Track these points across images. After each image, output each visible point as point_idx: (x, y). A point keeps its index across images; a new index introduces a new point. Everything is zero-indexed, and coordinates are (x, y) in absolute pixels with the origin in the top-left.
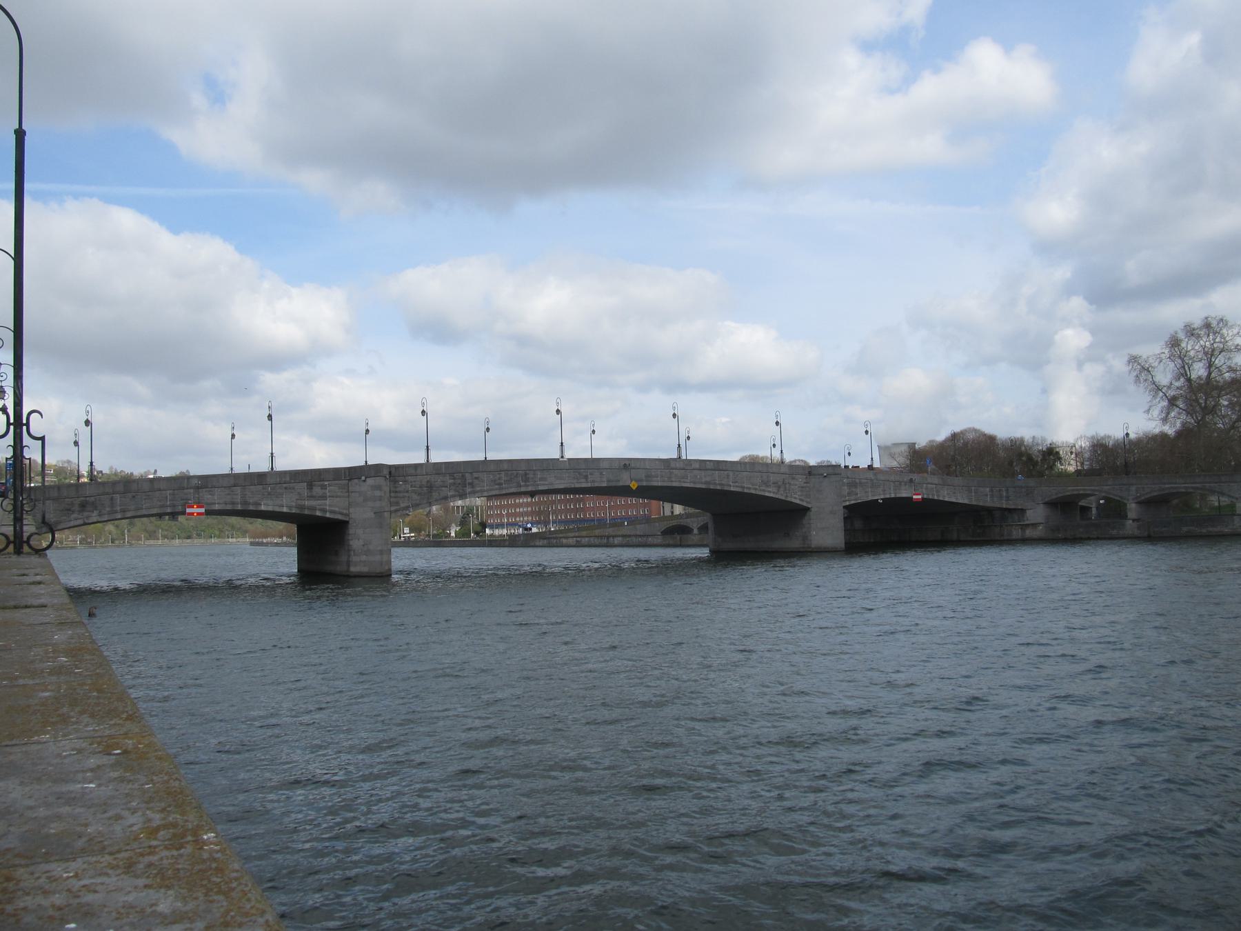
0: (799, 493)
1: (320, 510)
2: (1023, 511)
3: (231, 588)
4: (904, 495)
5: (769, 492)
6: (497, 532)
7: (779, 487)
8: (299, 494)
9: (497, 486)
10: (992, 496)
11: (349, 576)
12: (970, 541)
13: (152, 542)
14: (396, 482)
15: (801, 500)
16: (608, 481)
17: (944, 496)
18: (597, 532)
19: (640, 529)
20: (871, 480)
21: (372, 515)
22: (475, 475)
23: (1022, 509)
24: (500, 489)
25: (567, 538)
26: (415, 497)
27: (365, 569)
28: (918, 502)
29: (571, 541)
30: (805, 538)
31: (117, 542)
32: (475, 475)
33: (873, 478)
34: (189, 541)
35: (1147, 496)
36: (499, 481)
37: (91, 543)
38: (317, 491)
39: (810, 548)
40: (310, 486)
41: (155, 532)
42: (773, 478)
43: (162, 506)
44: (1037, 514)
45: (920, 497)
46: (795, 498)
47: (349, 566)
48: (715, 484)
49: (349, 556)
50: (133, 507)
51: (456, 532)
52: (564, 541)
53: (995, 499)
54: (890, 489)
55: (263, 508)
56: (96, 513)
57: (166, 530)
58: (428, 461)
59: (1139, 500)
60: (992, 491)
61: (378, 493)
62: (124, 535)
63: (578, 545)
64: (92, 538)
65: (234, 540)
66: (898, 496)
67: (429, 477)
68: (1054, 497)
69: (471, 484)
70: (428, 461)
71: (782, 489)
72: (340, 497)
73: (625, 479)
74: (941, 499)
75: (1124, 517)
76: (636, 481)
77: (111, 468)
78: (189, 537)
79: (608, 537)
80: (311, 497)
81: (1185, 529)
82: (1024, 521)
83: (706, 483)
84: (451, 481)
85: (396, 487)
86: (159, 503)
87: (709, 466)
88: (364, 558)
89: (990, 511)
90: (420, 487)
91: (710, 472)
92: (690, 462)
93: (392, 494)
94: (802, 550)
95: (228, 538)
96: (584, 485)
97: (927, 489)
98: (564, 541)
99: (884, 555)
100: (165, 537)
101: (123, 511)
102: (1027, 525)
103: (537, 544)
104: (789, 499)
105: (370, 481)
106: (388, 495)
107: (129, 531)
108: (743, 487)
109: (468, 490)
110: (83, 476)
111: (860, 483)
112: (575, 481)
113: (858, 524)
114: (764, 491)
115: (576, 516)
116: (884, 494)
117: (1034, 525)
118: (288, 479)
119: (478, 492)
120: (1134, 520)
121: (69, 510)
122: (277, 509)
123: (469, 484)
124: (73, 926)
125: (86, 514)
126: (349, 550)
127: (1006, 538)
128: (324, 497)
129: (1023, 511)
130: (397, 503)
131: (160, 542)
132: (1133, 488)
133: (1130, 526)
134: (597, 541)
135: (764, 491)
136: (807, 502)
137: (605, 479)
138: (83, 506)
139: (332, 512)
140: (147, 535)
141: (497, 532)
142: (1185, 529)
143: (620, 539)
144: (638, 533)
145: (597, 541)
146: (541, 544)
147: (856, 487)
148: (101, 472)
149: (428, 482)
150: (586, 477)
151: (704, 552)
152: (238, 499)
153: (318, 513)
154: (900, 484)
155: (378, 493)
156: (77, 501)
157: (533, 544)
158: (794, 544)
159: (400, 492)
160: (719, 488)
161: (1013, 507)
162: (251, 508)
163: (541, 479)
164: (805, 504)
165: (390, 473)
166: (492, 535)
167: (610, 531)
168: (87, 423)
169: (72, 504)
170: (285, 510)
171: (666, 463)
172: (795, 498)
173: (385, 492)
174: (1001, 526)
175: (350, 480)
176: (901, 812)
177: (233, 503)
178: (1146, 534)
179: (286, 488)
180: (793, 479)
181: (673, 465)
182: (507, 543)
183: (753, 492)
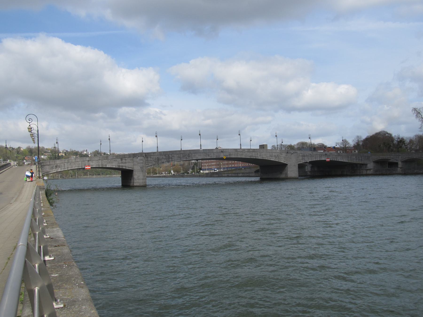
0: (283, 159)
1: (125, 167)
2: (366, 164)
3: (95, 189)
4: (323, 159)
5: (273, 159)
6: (205, 172)
7: (276, 157)
8: (118, 162)
9: (180, 159)
10: (356, 159)
11: (134, 186)
12: (351, 175)
13: (86, 177)
14: (147, 158)
15: (284, 161)
16: (216, 156)
17: (339, 160)
18: (234, 172)
19: (248, 171)
20: (311, 154)
21: (140, 168)
22: (173, 155)
23: (366, 164)
24: (180, 159)
25: (224, 174)
26: (154, 162)
27: (138, 184)
28: (328, 162)
29: (226, 175)
30: (286, 174)
31: (73, 177)
32: (173, 155)
33: (311, 153)
34: (99, 176)
35: (404, 160)
36: (180, 157)
37: (64, 177)
38: (124, 161)
39: (288, 177)
40: (122, 160)
41: (87, 173)
42: (274, 154)
43: (78, 166)
44: (371, 165)
45: (329, 160)
46: (282, 161)
47: (134, 183)
48: (253, 157)
49: (134, 180)
50: (70, 167)
51: (191, 171)
52: (223, 175)
53: (357, 160)
54: (318, 157)
55: (108, 166)
56: (60, 169)
57: (91, 172)
58: (158, 151)
59: (402, 161)
60: (356, 157)
61: (141, 161)
62: (76, 174)
63: (228, 176)
64: (64, 175)
65: (115, 175)
66: (321, 159)
67: (158, 156)
68: (376, 160)
69: (171, 158)
70: (158, 151)
71: (277, 158)
72: (131, 163)
73: (222, 156)
74: (338, 160)
75: (397, 166)
76: (225, 156)
77: (71, 149)
78: (99, 175)
79: (237, 173)
80: (122, 163)
81: (416, 171)
82: (367, 168)
83: (250, 156)
84: (165, 157)
85: (148, 159)
86: (78, 166)
87: (251, 151)
88: (138, 181)
89: (356, 164)
90: (155, 159)
91: (251, 153)
92: (160, 152)
93: (147, 162)
94: (285, 178)
95: (113, 175)
96: (208, 158)
97: (332, 157)
98: (223, 175)
99: (338, 178)
100: (90, 175)
101: (68, 168)
102: (368, 169)
103: (215, 176)
104: (280, 161)
105: (139, 158)
106: (145, 162)
107: (77, 173)
108: (263, 158)
109: (170, 160)
110: (60, 153)
111: (307, 156)
112: (205, 156)
113: (316, 169)
114: (271, 158)
115: (235, 165)
116: (316, 159)
117: (370, 169)
118: (115, 158)
119: (173, 160)
120: (400, 168)
121: (52, 168)
122: (112, 167)
123: (171, 158)
124: (82, 283)
125: (57, 169)
126: (134, 179)
127: (361, 174)
128: (126, 163)
129: (366, 164)
130: (148, 164)
131: (88, 177)
132: (400, 157)
133: (399, 170)
134: (234, 175)
135: (271, 158)
136: (286, 162)
137: (215, 156)
138: (56, 167)
139: (128, 167)
140: (84, 174)
141: (205, 172)
142: (416, 171)
143: (241, 174)
144: (247, 172)
145: (234, 175)
146: (216, 176)
147: (305, 157)
148: (67, 151)
149: (158, 158)
150: (209, 155)
151: (258, 179)
152: (100, 164)
153: (124, 168)
154: (322, 156)
155: (141, 161)
156: (55, 166)
157: (213, 176)
158: (283, 176)
159: (149, 161)
160: (254, 158)
161: (363, 163)
162: (104, 166)
163: (194, 156)
164: (285, 163)
165: (146, 155)
166: (203, 173)
167: (238, 171)
168: (57, 143)
169: (53, 166)
170: (114, 167)
171: (236, 150)
172: (282, 161)
173: (144, 161)
174: (360, 170)
175: (133, 157)
176: (374, 264)
177: (99, 165)
178: (404, 173)
179: (114, 160)
180: (282, 154)
181: (238, 151)
182: (205, 176)
183: (267, 159)
